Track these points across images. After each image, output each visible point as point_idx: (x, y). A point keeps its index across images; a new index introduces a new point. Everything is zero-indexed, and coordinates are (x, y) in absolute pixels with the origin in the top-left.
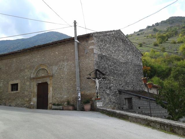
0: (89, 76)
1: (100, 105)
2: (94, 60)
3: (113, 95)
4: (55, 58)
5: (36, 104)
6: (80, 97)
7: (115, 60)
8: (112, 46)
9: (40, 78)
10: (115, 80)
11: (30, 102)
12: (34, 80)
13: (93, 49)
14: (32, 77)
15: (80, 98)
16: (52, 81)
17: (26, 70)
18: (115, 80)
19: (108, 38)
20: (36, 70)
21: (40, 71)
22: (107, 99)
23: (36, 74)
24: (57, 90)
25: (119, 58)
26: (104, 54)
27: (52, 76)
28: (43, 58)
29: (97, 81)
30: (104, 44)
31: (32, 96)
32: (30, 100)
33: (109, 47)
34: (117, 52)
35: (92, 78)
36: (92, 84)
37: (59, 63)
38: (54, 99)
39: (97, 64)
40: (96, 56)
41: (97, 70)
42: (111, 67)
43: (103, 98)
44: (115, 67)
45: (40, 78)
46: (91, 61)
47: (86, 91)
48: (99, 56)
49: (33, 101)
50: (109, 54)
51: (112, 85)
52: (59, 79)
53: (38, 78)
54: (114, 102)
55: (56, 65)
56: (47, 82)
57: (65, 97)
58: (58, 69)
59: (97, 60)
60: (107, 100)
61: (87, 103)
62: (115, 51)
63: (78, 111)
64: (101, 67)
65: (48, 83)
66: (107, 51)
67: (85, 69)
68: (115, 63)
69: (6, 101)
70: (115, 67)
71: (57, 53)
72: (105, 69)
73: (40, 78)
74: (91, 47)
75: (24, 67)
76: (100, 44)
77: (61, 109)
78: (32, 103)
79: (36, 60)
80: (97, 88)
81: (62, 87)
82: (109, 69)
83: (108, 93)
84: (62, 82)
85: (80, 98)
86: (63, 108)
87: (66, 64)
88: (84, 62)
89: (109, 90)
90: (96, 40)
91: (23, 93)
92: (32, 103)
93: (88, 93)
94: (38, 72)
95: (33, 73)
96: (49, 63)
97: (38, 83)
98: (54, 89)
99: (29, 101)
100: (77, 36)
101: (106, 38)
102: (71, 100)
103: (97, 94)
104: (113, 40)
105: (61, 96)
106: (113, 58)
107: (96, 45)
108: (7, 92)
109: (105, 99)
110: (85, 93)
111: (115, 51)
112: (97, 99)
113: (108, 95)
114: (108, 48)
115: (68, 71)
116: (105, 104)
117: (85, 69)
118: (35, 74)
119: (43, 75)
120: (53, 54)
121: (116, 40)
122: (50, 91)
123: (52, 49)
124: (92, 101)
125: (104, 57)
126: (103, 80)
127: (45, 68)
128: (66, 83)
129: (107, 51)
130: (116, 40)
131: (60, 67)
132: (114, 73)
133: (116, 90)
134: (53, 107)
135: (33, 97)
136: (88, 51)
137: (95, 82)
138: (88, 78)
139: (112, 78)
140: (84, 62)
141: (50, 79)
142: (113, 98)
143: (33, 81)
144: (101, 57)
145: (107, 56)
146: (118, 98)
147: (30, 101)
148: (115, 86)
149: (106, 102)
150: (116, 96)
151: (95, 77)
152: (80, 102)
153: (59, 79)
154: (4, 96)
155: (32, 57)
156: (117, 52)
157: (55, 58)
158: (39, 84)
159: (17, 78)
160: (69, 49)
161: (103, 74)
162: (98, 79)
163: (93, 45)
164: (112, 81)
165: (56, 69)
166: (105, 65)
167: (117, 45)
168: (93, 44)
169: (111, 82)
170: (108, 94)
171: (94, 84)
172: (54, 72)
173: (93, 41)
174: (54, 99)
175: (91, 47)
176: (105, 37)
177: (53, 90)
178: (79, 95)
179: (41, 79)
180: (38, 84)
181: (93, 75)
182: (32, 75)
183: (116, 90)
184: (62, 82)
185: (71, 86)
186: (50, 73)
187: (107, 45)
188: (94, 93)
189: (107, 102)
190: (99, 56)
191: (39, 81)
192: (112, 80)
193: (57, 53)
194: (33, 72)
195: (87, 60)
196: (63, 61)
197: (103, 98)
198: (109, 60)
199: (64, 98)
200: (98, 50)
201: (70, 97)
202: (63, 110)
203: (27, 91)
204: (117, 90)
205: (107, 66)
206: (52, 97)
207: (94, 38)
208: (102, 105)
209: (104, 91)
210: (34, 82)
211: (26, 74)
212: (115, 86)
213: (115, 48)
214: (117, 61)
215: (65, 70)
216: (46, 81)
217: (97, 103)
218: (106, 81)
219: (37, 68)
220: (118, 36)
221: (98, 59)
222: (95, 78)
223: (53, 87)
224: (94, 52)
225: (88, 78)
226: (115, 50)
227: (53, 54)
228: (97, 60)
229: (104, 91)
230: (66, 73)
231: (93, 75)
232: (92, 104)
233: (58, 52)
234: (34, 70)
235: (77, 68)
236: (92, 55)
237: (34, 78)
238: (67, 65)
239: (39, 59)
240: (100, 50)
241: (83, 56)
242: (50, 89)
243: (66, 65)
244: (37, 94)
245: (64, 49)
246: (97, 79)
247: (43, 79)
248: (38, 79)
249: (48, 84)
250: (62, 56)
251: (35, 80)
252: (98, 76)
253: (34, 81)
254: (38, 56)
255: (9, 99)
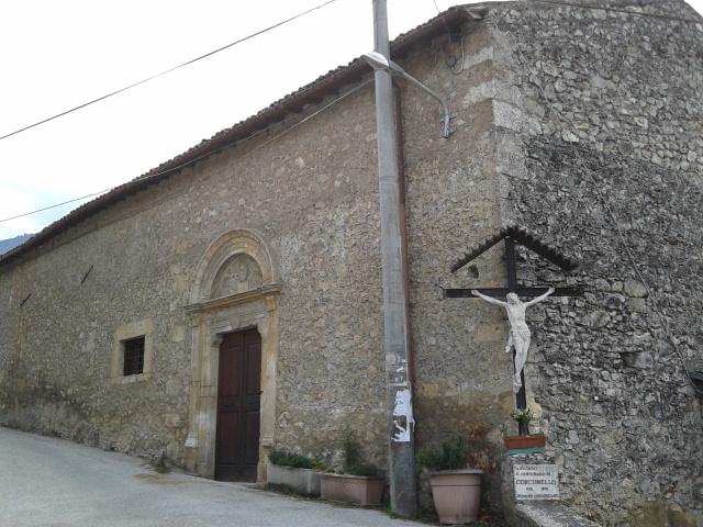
0: (463, 277)
1: (537, 490)
2: (498, 169)
3: (652, 406)
4: (290, 194)
5: (209, 446)
6: (410, 420)
7: (658, 179)
8: (632, 88)
9: (225, 305)
10: (662, 304)
11: (185, 437)
13: (491, 99)
15: (404, 424)
16: (277, 321)
17: (175, 269)
18: (662, 304)
19: (602, 40)
21: (230, 267)
22: (608, 439)
23: (214, 283)
24: (300, 368)
25: (685, 164)
26: (574, 139)
27: (276, 293)
28: (242, 201)
29: (517, 309)
30: (570, 75)
31: (194, 400)
32: (184, 427)
33: (611, 94)
34: (668, 130)
35: (480, 290)
36: (484, 335)
37: (309, 217)
38: (284, 424)
39: (515, 197)
40: (510, 146)
41: (513, 236)
42: (628, 217)
43: (573, 434)
44: (659, 220)
45: (225, 305)
46: (476, 179)
47: (451, 381)
48: (531, 146)
49: (197, 427)
50: (608, 140)
51: (638, 337)
52: (309, 304)
54: (661, 461)
55: (295, 229)
57: (338, 412)
58: (302, 249)
59: (521, 172)
60: (607, 447)
61: (447, 468)
62: (655, 121)
63: (395, 516)
64: (551, 221)
65: (259, 330)
66: (596, 119)
67: (440, 237)
68: (658, 197)
69: (101, 425)
70: (659, 220)
71: (301, 162)
72: (584, 229)
73: (228, 306)
74: (476, 94)
75: (168, 252)
76: (542, 75)
77: (309, 490)
78: (191, 442)
79: (213, 213)
80: (520, 361)
81: (325, 353)
82: (616, 232)
83: (611, 392)
84: (322, 322)
85: (404, 424)
86: (319, 486)
87: (339, 216)
88: (435, 197)
89: (615, 376)
90: (509, 49)
91: (162, 386)
92: (191, 442)
93: (462, 391)
96: (266, 219)
97: (218, 334)
98: (285, 368)
99: (181, 428)
100: (392, 36)
101: (582, 38)
102: (370, 436)
103: (522, 402)
104: (633, 54)
105: (316, 407)
106: (644, 166)
107: (511, 75)
108: (108, 377)
109: (589, 438)
110: (448, 394)
111: (655, 121)
112: (526, 441)
113: (613, 407)
114: (600, 103)
115: (351, 260)
116: (590, 475)
117: (440, 237)
118: (210, 282)
119: (243, 288)
120: (283, 169)
121: (661, 53)
122: (268, 378)
123: (281, 147)
124: (492, 450)
125: (572, 156)
126: (573, 307)
128: (343, 331)
129: (596, 119)
130: (661, 53)
131: (314, 240)
132: (656, 263)
133: (678, 377)
134: (276, 474)
135: (199, 406)
136: (461, 122)
137: (503, 318)
138: (452, 293)
139: (640, 290)
140: (435, 197)
141: (269, 308)
142: (656, 428)
144: (552, 155)
145: (600, 147)
146: (690, 426)
147: (184, 432)
148: (661, 345)
149: (600, 460)
150: (678, 415)
151: (502, 284)
152: (405, 453)
153: (309, 304)
154: (96, 398)
155: (197, 199)
156: (668, 130)
157: (290, 194)
158: (226, 336)
159: (141, 312)
160: (358, 128)
161: (567, 266)
162: (526, 293)
163: (489, 79)
164: (643, 315)
165: (296, 249)
166: (581, 206)
167: (665, 86)
168: (487, 70)
169: (634, 316)
170: (614, 400)
171: (497, 335)
172: (286, 267)
173: (487, 53)
174: (284, 424)
175: (476, 94)
176: (578, 33)
177: (279, 372)
178: (403, 406)
179: (232, 311)
180: (221, 340)
181: (490, 275)
183: (678, 377)
184: (322, 322)
185: (366, 345)
186: (270, 276)
187: (597, 81)
188: (502, 397)
189: (608, 457)
190: (531, 146)
192: (641, 305)
193: (301, 162)
194: (200, 275)
195: (453, 177)
196: (330, 200)
197: (573, 434)
198: (617, 176)
199: (334, 423)
200: (529, 112)
201: (362, 417)
202: (314, 496)
203: (175, 374)
204: (683, 371)
205: (595, 211)
206: (278, 412)
207: (497, 33)
208: (553, 490)
209: (578, 378)
210: (204, 325)
211: (174, 285)
212: (661, 345)
213: (652, 101)
214: (672, 185)
215: (339, 250)
217: (520, 473)
218: (594, 316)
219: (217, 255)
220: (669, 31)
221: (529, 166)
222: (500, 293)
223: (279, 353)
224: (498, 122)
225: (452, 293)
226: (654, 114)
227: (283, 169)
228: (521, 172)
229: (578, 378)
230: (344, 270)
231: (490, 266)
232: (492, 470)
233: (305, 157)
234: (205, 263)
235: (388, 232)
236: (484, 140)
237: (201, 309)
238: (347, 222)
239: (226, 204)
240: (540, 110)
241: (429, 156)
242: (270, 364)
243: (341, 223)
244: (215, 390)
245: (335, 136)
246: (513, 296)
248: (220, 314)
249: (259, 336)
250: (323, 178)
251: (209, 316)
252: (528, 279)
253: (202, 321)
254: (223, 193)
255: (113, 414)
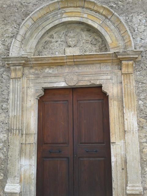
12: (26, 71)
14: (14, 53)
20: (36, 25)
53: (50, 65)
56: (100, 87)
65: (104, 89)
94: (42, 37)
95: (19, 38)
127: (90, 23)
143: (19, 74)
179: (66, 70)
182: (17, 44)
191: (55, 76)
210: (25, 79)
216: (98, 83)
219: (44, 18)
234: (30, 23)
247: (76, 69)
249: (105, 97)
